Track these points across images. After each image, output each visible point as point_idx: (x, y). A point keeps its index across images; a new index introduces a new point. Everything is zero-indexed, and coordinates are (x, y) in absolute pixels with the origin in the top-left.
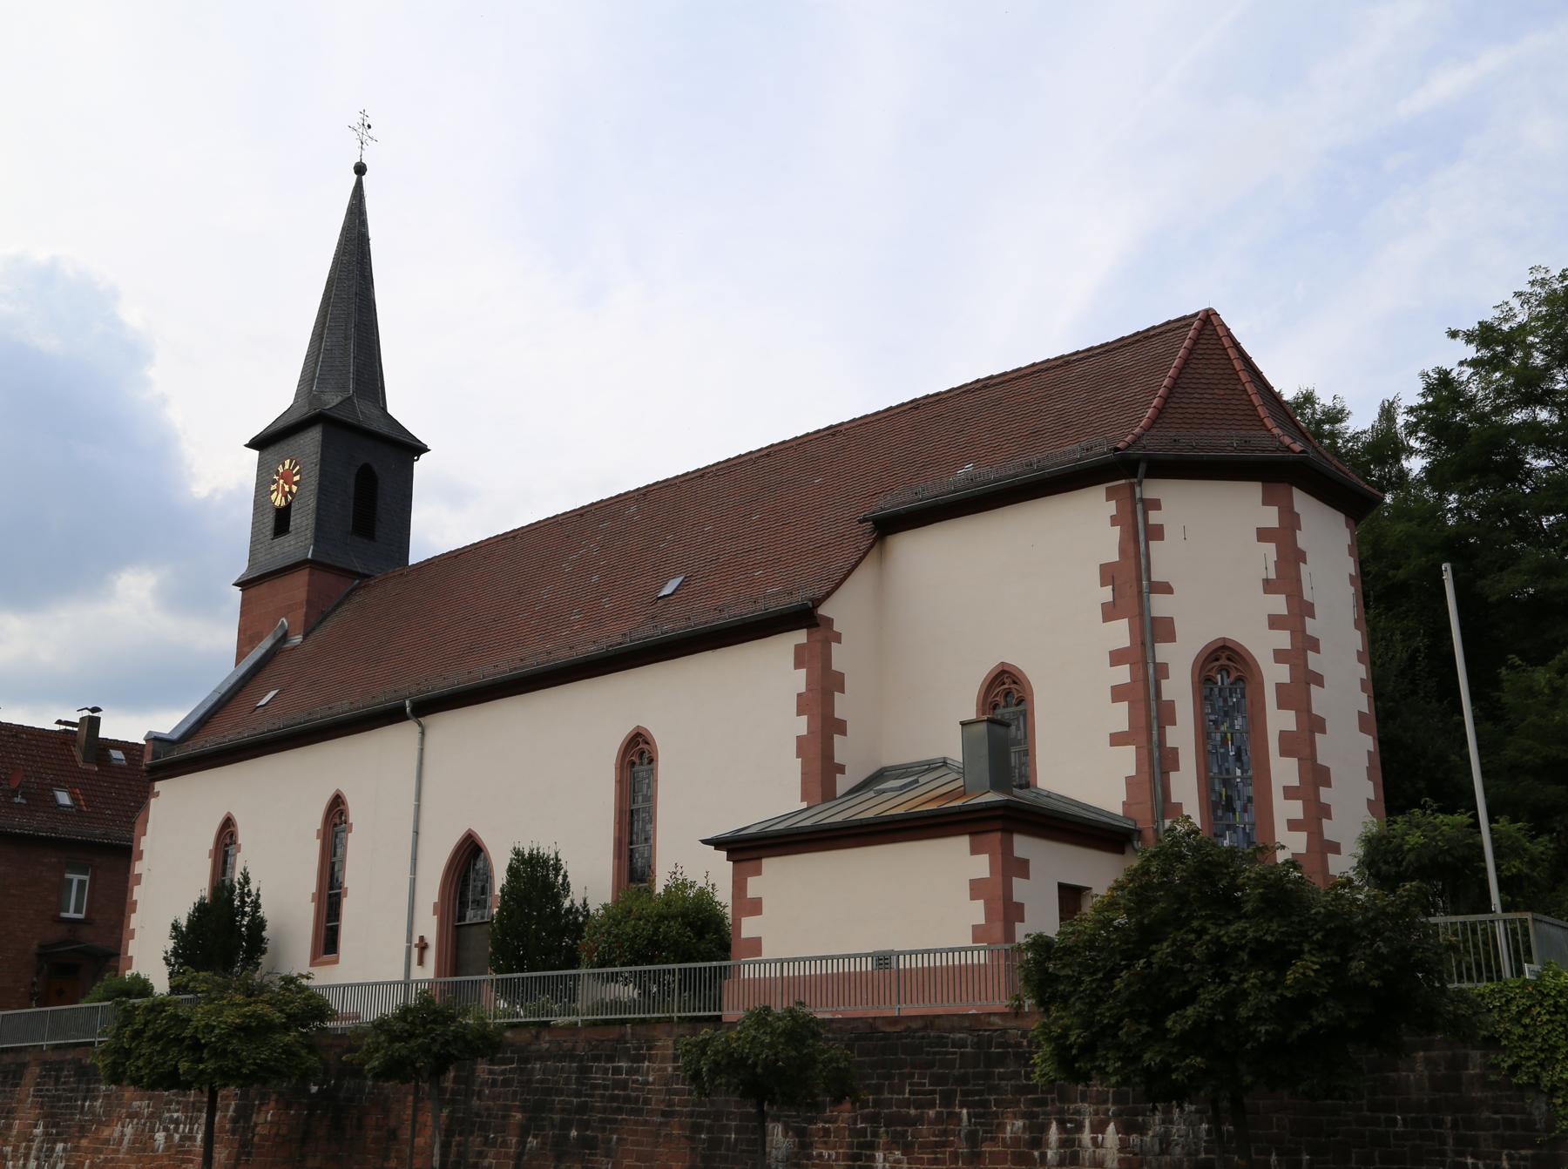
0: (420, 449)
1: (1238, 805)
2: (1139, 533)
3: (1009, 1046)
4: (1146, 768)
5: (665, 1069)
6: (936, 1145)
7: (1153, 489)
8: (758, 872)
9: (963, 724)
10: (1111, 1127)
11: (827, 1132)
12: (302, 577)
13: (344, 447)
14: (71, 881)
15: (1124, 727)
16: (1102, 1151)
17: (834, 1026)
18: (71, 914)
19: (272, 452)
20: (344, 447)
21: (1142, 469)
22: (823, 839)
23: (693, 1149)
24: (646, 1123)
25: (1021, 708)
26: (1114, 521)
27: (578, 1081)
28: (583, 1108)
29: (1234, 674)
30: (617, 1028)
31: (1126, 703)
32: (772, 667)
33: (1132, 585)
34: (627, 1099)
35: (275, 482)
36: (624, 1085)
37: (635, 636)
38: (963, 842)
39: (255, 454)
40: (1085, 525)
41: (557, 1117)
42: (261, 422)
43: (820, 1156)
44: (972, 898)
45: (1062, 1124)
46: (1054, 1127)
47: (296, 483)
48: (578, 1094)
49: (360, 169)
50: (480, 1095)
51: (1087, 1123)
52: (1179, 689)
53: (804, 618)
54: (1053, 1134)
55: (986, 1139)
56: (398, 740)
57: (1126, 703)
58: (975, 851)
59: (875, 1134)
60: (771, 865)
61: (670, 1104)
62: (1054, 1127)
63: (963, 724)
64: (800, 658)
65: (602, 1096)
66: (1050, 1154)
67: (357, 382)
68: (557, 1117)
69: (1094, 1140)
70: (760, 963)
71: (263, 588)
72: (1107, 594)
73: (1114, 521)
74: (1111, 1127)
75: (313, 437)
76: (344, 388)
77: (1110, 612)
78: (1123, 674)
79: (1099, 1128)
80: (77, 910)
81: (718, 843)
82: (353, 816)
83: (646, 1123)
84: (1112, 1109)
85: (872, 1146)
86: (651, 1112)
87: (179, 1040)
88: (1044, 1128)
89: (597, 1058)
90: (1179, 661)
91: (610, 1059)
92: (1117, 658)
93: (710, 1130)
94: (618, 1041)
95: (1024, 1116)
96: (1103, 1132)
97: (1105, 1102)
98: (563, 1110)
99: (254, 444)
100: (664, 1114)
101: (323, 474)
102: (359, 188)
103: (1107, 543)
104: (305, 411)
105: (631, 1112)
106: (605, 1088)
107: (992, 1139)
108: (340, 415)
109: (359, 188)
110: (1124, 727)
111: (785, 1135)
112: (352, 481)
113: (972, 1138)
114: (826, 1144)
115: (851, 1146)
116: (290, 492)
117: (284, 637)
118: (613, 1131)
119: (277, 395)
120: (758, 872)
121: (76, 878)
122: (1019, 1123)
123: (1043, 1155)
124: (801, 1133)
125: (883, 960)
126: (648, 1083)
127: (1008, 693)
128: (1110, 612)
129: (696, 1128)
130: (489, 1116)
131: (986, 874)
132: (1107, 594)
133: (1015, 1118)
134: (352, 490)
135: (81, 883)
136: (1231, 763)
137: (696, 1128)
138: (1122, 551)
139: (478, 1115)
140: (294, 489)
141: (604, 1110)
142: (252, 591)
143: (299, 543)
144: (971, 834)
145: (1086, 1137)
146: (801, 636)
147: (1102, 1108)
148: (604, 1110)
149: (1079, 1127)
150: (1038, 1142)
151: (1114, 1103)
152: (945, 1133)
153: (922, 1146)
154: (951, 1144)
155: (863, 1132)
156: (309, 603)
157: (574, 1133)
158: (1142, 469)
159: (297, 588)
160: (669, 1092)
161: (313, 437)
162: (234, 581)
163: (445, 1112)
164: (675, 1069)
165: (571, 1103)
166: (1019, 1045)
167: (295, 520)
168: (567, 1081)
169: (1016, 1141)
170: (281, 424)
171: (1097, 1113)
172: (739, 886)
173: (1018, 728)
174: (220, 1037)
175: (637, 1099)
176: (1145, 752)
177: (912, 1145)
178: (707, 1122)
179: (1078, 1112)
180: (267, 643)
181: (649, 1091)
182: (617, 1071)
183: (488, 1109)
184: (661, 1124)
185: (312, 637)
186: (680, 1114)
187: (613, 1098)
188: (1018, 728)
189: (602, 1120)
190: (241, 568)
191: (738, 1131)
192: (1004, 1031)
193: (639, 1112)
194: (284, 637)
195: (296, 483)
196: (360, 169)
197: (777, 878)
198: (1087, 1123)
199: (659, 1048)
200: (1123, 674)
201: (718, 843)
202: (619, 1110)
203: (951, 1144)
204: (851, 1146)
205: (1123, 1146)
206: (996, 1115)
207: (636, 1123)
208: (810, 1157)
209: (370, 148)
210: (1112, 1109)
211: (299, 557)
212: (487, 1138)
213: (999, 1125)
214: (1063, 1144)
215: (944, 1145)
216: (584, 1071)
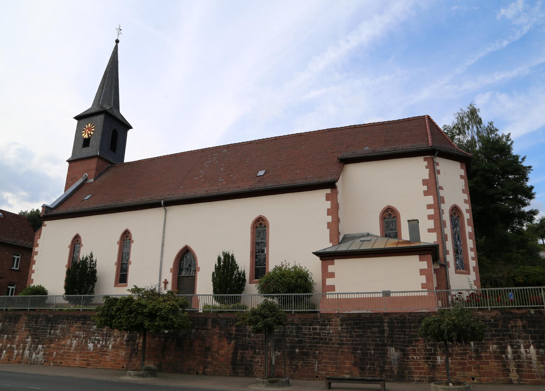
0: (130, 127)
1: (459, 252)
2: (434, 172)
3: (486, 321)
4: (440, 239)
5: (338, 329)
6: (462, 354)
7: (438, 160)
8: (333, 264)
9: (408, 221)
10: (532, 347)
11: (414, 350)
12: (94, 161)
13: (105, 124)
14: (15, 258)
15: (433, 227)
16: (530, 355)
17: (412, 315)
18: (14, 268)
19: (83, 121)
20: (105, 124)
21: (437, 153)
22: (372, 254)
23: (355, 356)
24: (331, 347)
25: (394, 219)
26: (427, 167)
27: (296, 332)
28: (300, 342)
29: (457, 215)
30: (313, 314)
31: (433, 220)
32: (318, 200)
33: (432, 186)
34: (321, 339)
35: (84, 130)
36: (319, 334)
37: (210, 192)
38: (417, 257)
39: (76, 121)
40: (418, 167)
41: (288, 345)
42: (80, 111)
43: (413, 358)
44: (421, 275)
45: (512, 346)
46: (509, 347)
47: (93, 131)
48: (297, 337)
49: (117, 41)
50: (249, 336)
51: (522, 346)
52: (446, 217)
53: (332, 185)
54: (509, 349)
55: (482, 352)
56: (156, 214)
57: (433, 220)
58: (421, 260)
59: (435, 350)
60: (337, 261)
61: (342, 341)
62: (509, 347)
63: (408, 221)
64: (328, 198)
65: (309, 338)
66: (509, 356)
67: (114, 104)
68: (288, 345)
69: (526, 352)
70: (335, 294)
71: (78, 163)
72: (425, 188)
73: (427, 167)
74: (532, 347)
75: (101, 117)
76: (110, 105)
77: (426, 193)
78: (432, 212)
79: (527, 347)
80: (16, 267)
81: (317, 254)
82: (83, 242)
83: (331, 347)
84: (531, 341)
85: (435, 354)
86: (333, 343)
87: (142, 313)
88: (506, 348)
89: (305, 325)
90: (446, 208)
91: (312, 325)
92: (429, 207)
93: (361, 349)
94: (313, 319)
95: (496, 344)
96: (529, 349)
97: (528, 339)
98: (291, 342)
99: (77, 118)
100: (339, 344)
101: (103, 129)
102: (116, 48)
103: (425, 174)
104: (97, 109)
105: (324, 343)
106: (310, 335)
107: (485, 352)
108: (110, 112)
109: (116, 48)
110: (433, 227)
111: (396, 351)
112: (111, 133)
113: (476, 351)
114: (415, 354)
115: (426, 354)
116: (90, 134)
117: (86, 180)
118: (316, 350)
119: (86, 104)
120: (333, 264)
121: (16, 257)
122: (495, 346)
123: (507, 357)
124: (403, 350)
125: (387, 294)
126: (330, 333)
127: (390, 215)
128: (426, 193)
129: (355, 349)
130: (255, 344)
131: (426, 267)
132: (425, 188)
133: (493, 344)
134: (111, 136)
135: (18, 259)
136: (457, 240)
137: (355, 349)
138: (430, 176)
139: (249, 343)
140: (92, 133)
141: (311, 343)
142: (74, 164)
143: (94, 149)
144: (419, 255)
145: (522, 350)
146: (328, 191)
147: (527, 341)
148: (311, 343)
149: (519, 347)
150: (504, 351)
151: (531, 339)
152: (465, 350)
153: (456, 354)
154: (468, 353)
155: (430, 350)
156: (96, 169)
157: (297, 350)
158: (437, 153)
159: (93, 163)
160: (340, 336)
161: (101, 117)
162: (67, 159)
163: (233, 342)
164: (342, 329)
165: (295, 340)
166: (491, 321)
167: (92, 143)
168: (291, 332)
169: (495, 352)
170: (89, 112)
171: (525, 342)
172: (324, 269)
173: (393, 225)
174: (165, 313)
175: (326, 339)
176: (440, 235)
177: (452, 354)
178: (360, 347)
179: (518, 342)
180: (81, 181)
181: (331, 336)
182: (316, 329)
183: (254, 341)
184: (338, 348)
185: (98, 180)
186: (347, 344)
187: (314, 338)
188: (393, 225)
189: (309, 346)
190: (69, 156)
191: (374, 350)
192: (484, 316)
193: (328, 343)
194: (86, 180)
195: (93, 131)
196: (117, 41)
197: (339, 266)
198: (522, 346)
199: (333, 321)
200: (432, 212)
201: (317, 254)
202: (319, 343)
203: (468, 353)
204: (426, 354)
205: (538, 353)
206: (485, 344)
207: (327, 347)
208: (408, 359)
209: (120, 36)
210: (531, 341)
211: (93, 154)
212: (255, 352)
213: (487, 347)
214: (513, 353)
215: (466, 354)
216: (299, 329)
